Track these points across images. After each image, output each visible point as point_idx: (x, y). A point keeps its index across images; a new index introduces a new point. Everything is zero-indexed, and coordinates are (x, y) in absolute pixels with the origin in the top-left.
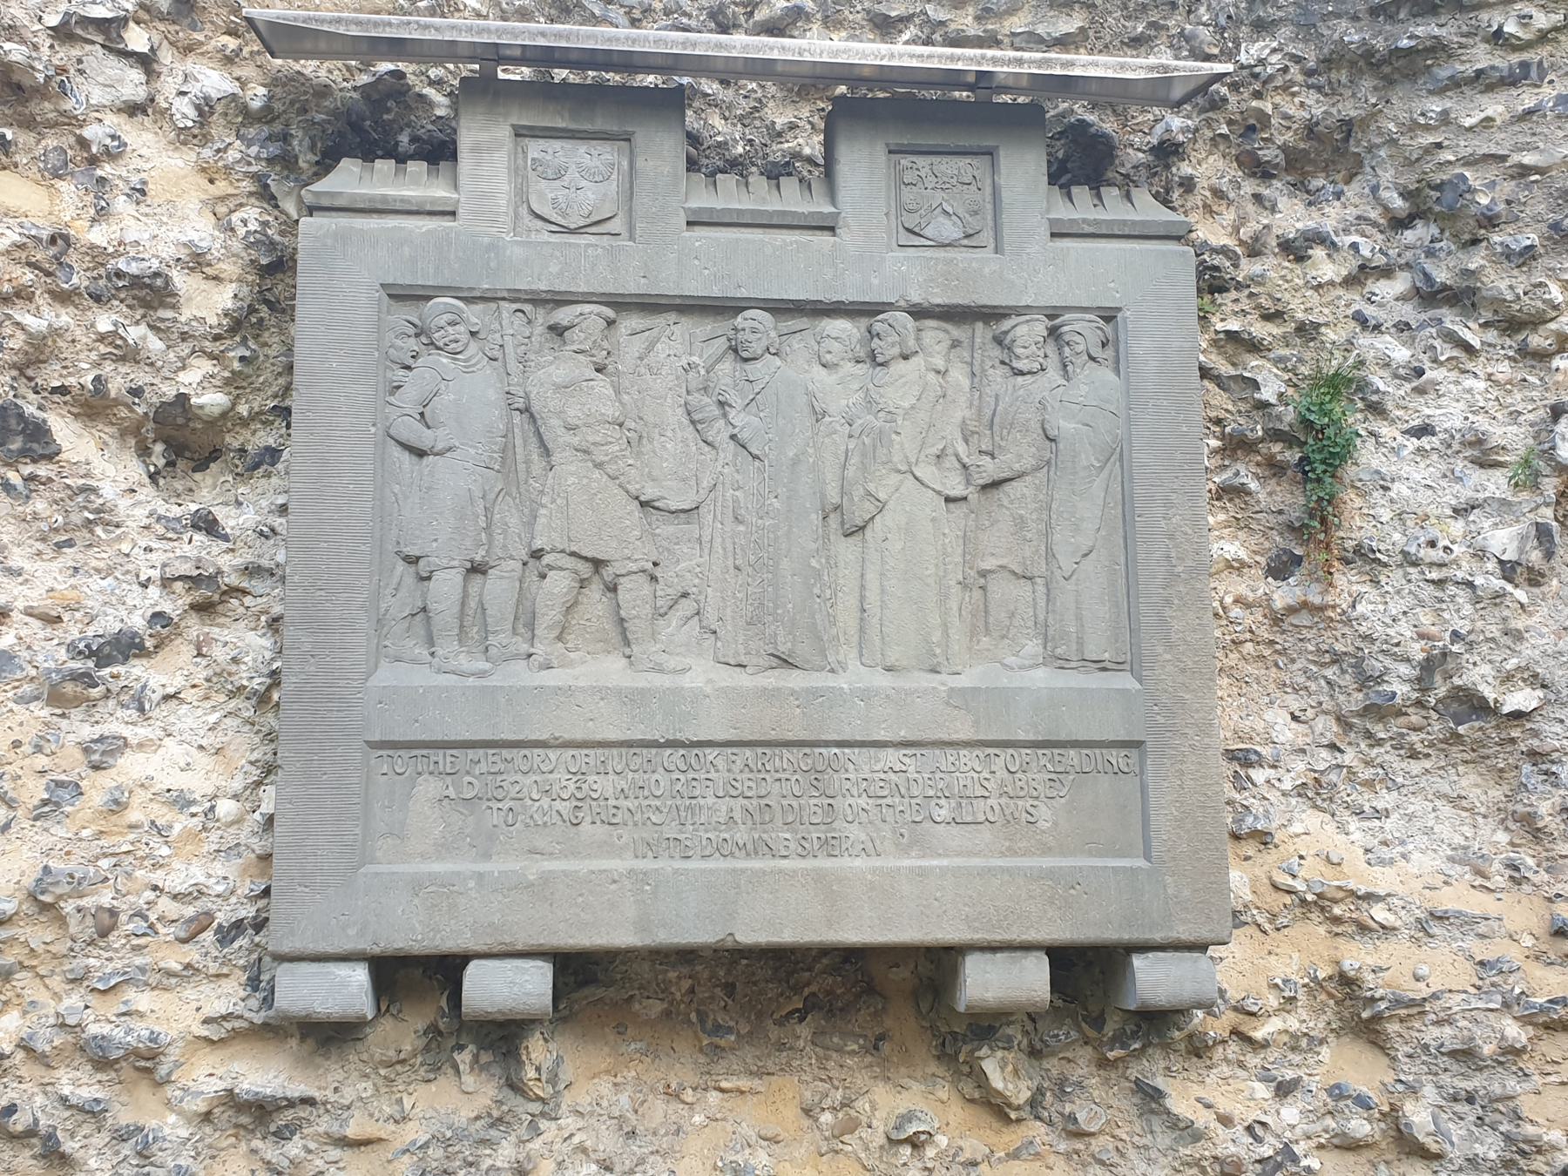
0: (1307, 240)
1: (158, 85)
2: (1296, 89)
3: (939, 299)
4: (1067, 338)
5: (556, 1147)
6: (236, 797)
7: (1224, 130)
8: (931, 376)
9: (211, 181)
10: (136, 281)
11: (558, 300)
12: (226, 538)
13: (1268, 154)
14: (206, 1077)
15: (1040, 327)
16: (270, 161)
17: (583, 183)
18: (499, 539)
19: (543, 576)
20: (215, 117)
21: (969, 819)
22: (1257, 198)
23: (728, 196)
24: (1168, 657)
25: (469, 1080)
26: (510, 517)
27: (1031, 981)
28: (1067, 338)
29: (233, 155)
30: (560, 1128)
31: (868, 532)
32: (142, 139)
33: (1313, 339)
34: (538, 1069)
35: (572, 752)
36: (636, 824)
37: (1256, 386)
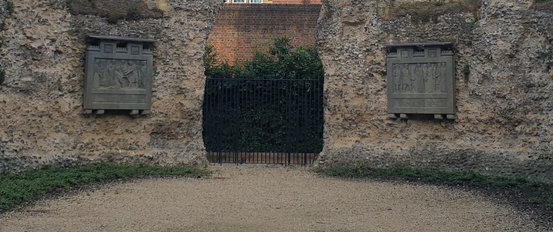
14: (386, 122)
27: (137, 112)
32: (377, 51)
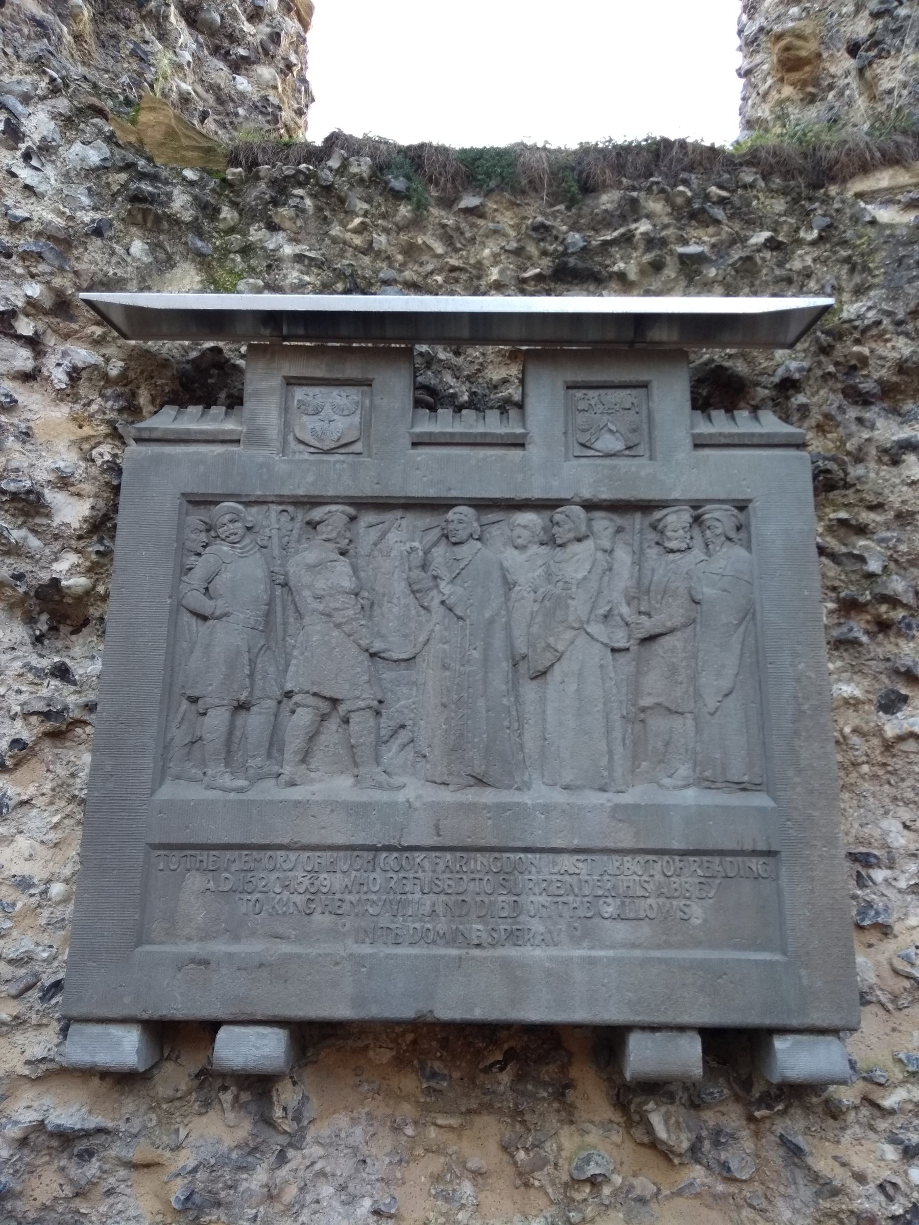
0: (901, 447)
1: (44, 360)
2: (888, 336)
3: (605, 494)
4: (708, 523)
5: (301, 1173)
6: (66, 881)
7: (831, 369)
8: (600, 555)
9: (81, 427)
10: (15, 496)
11: (313, 502)
12: (74, 683)
13: (867, 386)
15: (686, 516)
16: (120, 411)
17: (336, 417)
18: (259, 683)
19: (293, 712)
20: (81, 382)
21: (632, 915)
22: (860, 421)
23: (444, 423)
24: (798, 780)
25: (231, 1116)
26: (268, 666)
27: (689, 1055)
28: (708, 523)
29: (94, 407)
30: (304, 1158)
31: (549, 676)
33: (909, 524)
34: (285, 1109)
35: (309, 854)
36: (357, 915)
37: (862, 559)
